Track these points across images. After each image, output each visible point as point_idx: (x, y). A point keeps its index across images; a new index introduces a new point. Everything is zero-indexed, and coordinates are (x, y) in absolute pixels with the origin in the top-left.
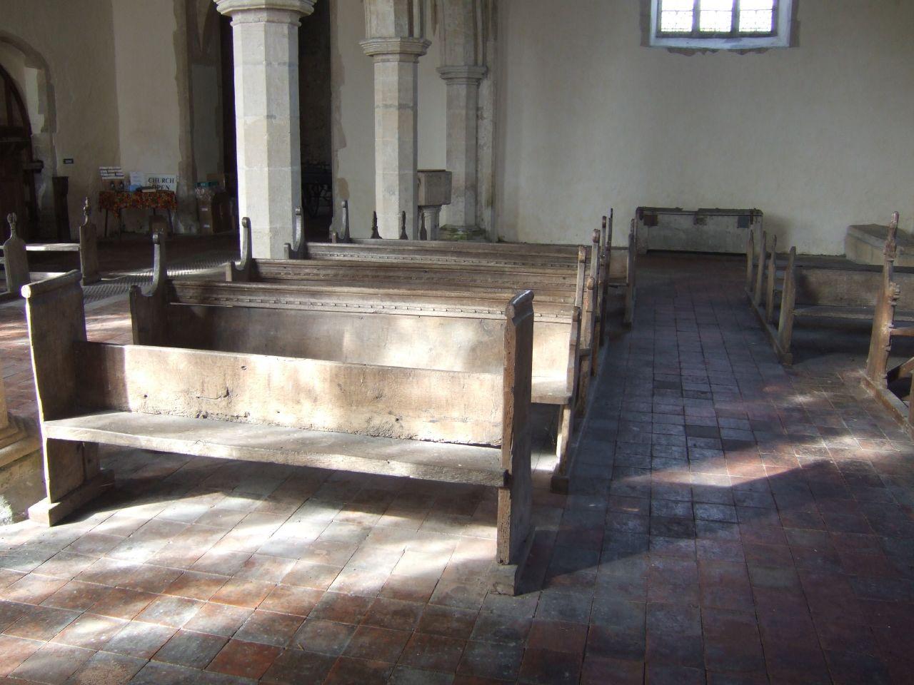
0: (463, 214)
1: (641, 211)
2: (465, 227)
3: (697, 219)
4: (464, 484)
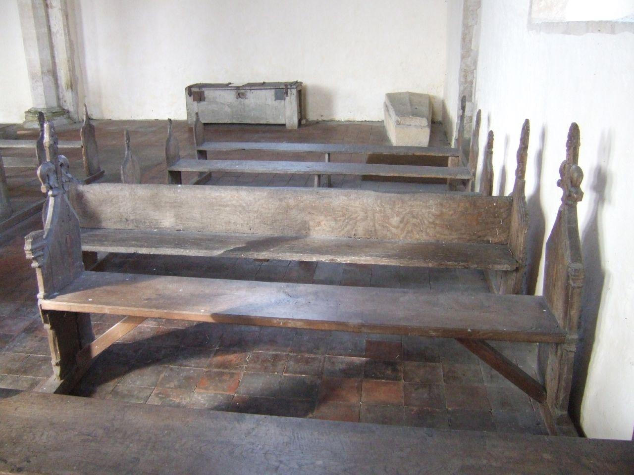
0: (44, 98)
1: (190, 90)
2: (47, 109)
3: (239, 94)
4: (90, 324)
